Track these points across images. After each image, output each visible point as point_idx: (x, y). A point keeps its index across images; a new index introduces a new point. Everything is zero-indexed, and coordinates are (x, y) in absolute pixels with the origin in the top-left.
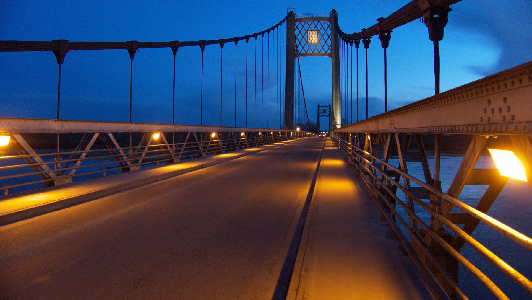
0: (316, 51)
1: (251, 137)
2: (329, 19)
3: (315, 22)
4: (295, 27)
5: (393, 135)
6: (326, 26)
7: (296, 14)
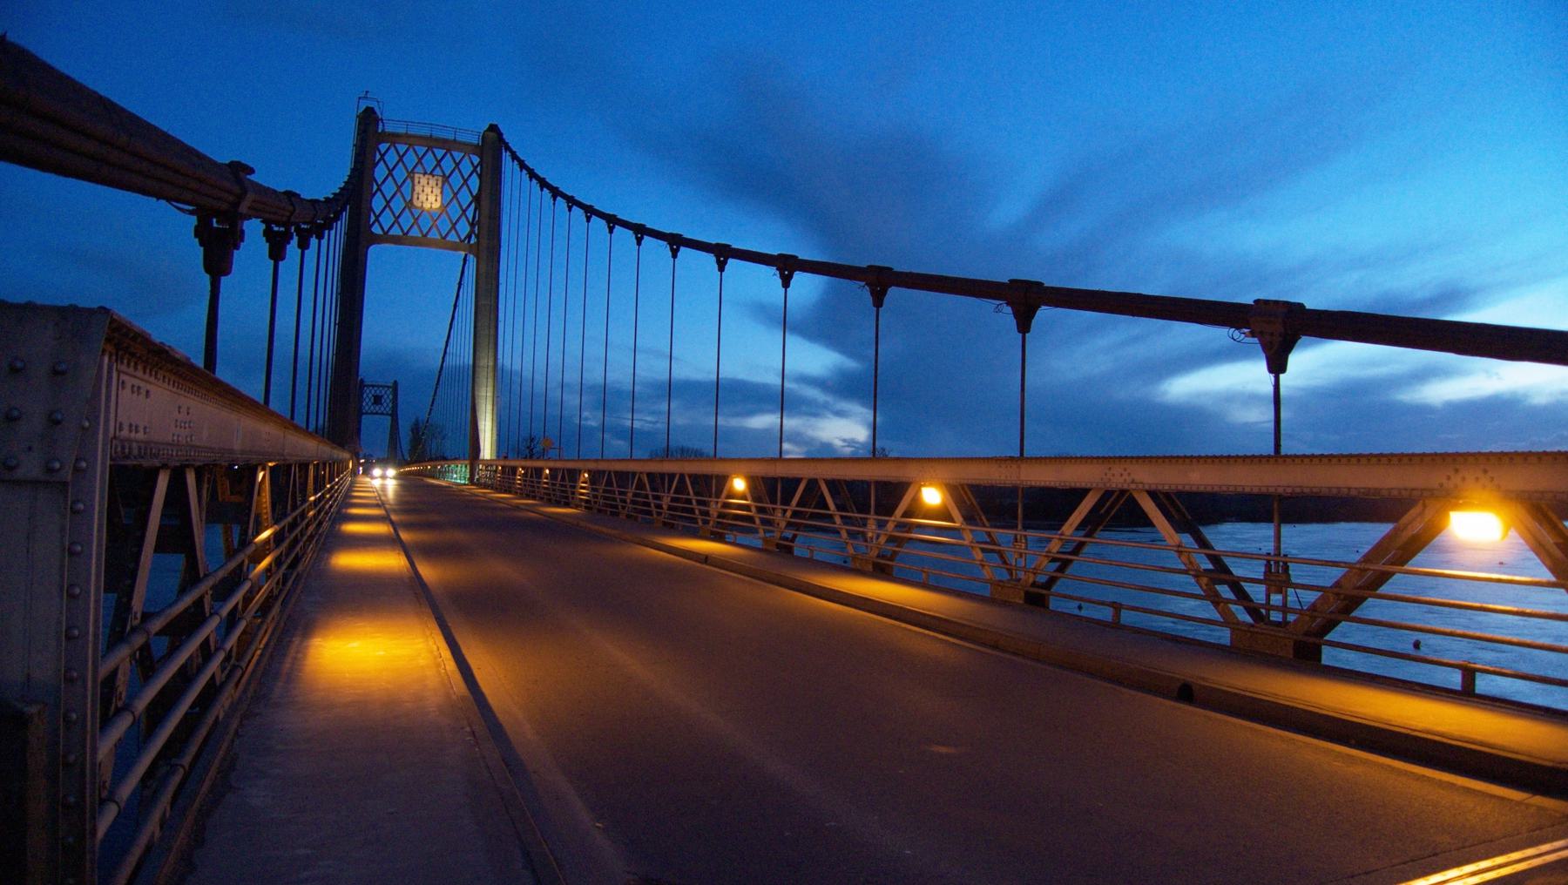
0: (434, 235)
2: (479, 150)
3: (398, 146)
4: (375, 157)
5: (610, 472)
6: (466, 168)
7: (382, 120)
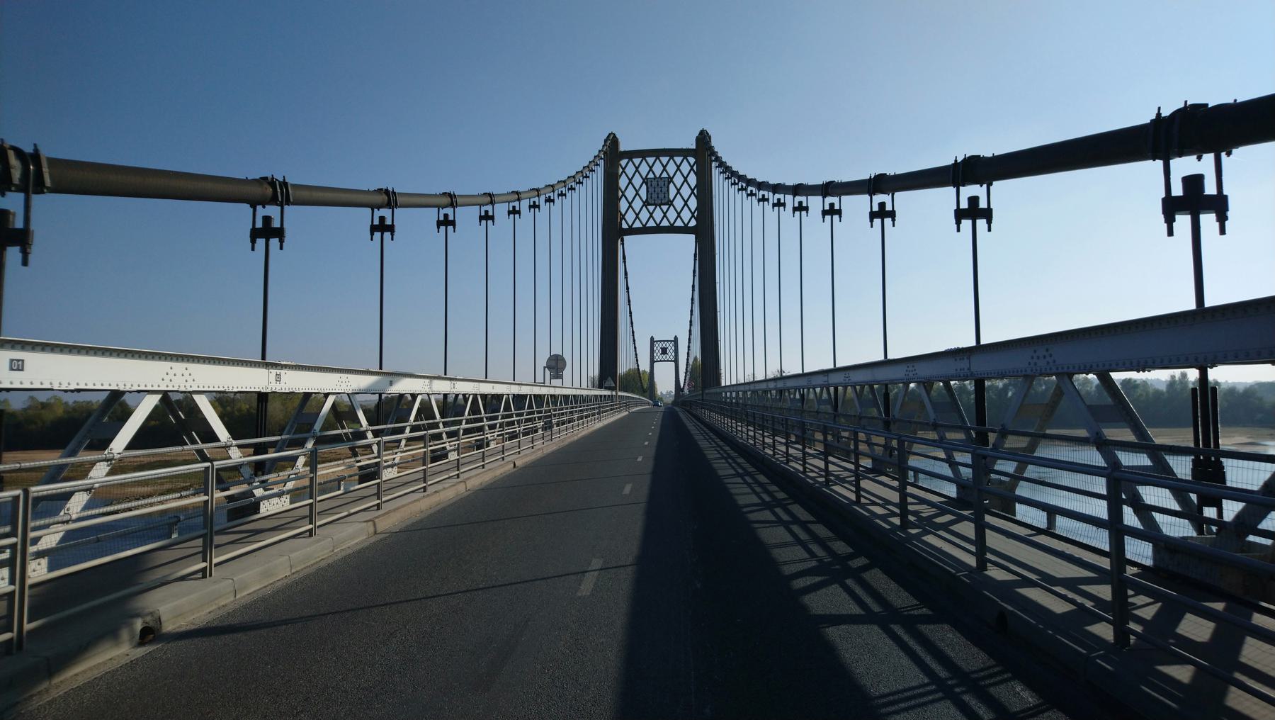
1: (467, 413)
